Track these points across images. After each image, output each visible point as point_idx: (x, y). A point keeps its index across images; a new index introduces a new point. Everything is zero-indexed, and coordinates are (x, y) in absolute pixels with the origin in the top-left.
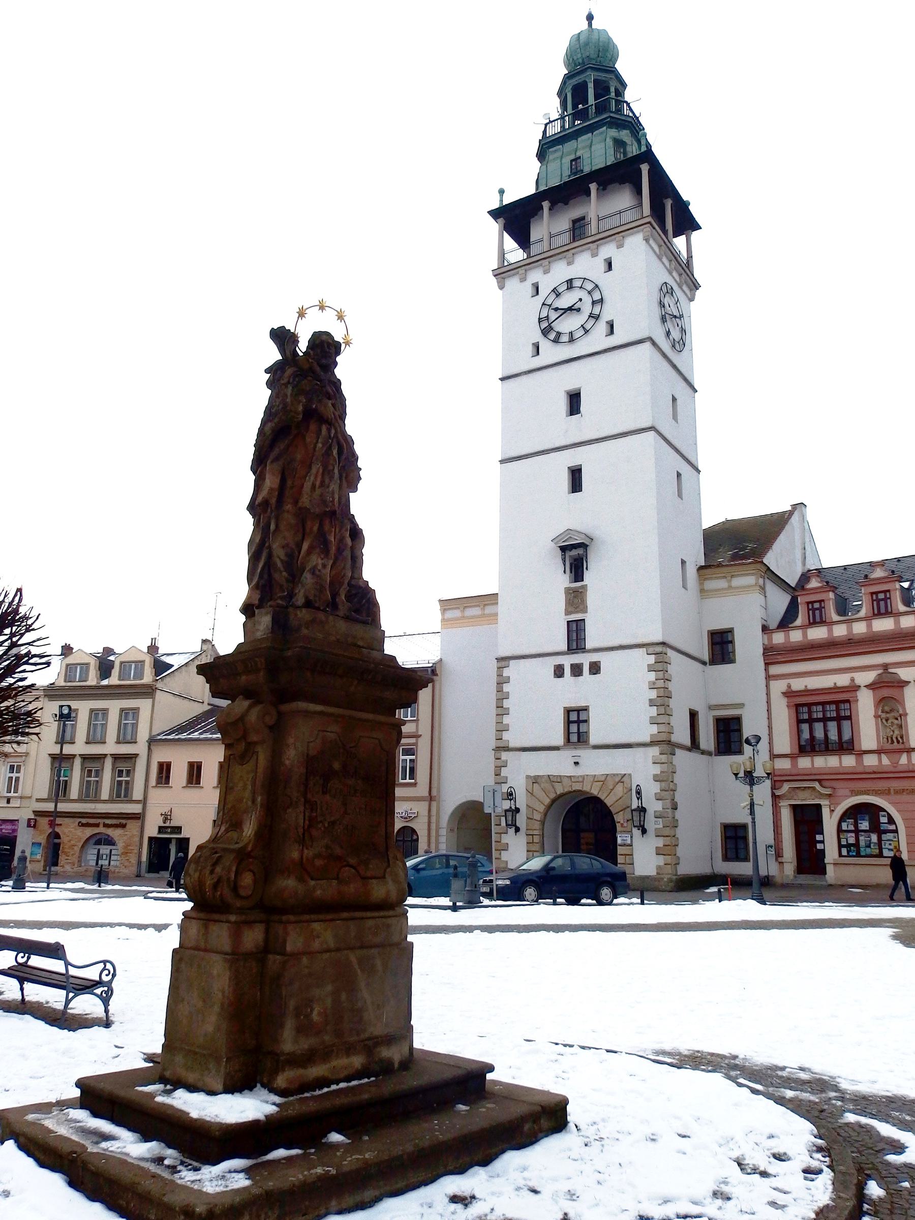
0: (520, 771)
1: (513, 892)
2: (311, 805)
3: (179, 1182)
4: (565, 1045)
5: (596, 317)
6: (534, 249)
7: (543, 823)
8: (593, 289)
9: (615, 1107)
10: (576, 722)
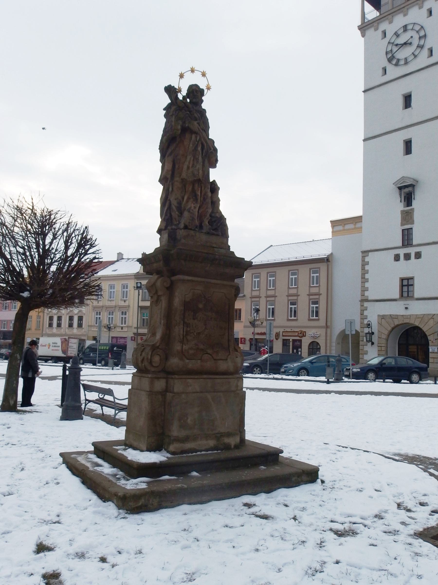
0: (374, 313)
1: (362, 375)
2: (186, 324)
3: (118, 484)
4: (343, 447)
5: (421, 47)
6: (383, 9)
7: (387, 340)
8: (420, 29)
9: (351, 476)
10: (406, 285)
